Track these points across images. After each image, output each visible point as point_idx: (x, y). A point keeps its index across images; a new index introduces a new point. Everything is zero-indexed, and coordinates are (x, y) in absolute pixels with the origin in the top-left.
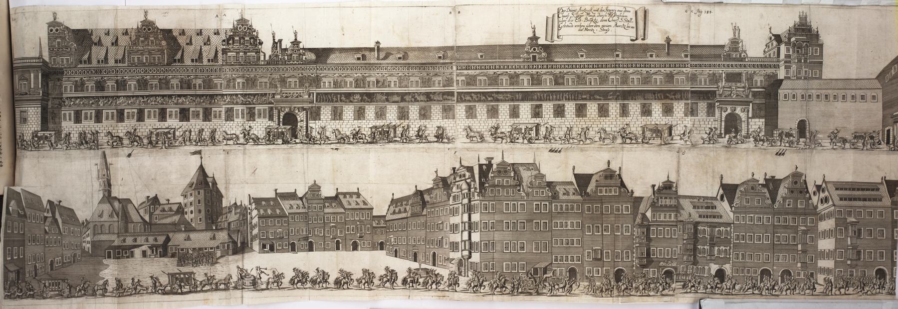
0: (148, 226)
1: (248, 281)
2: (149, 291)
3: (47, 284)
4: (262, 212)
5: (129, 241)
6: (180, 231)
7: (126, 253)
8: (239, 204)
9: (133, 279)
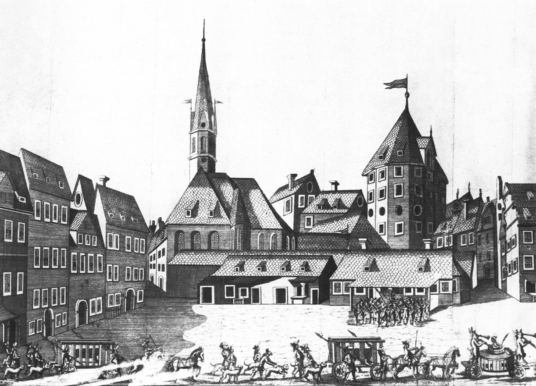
0: (291, 239)
1: (496, 362)
2: (289, 375)
3: (71, 353)
4: (526, 213)
5: (251, 269)
6: (357, 250)
7: (244, 293)
8: (475, 195)
9: (256, 348)
